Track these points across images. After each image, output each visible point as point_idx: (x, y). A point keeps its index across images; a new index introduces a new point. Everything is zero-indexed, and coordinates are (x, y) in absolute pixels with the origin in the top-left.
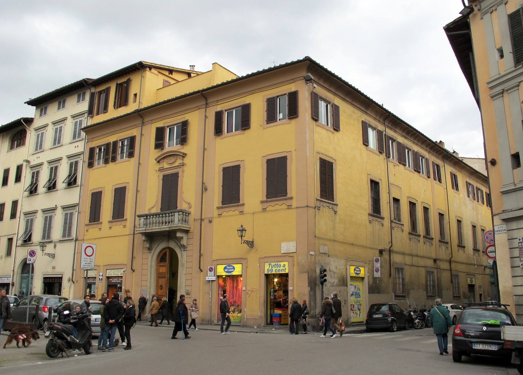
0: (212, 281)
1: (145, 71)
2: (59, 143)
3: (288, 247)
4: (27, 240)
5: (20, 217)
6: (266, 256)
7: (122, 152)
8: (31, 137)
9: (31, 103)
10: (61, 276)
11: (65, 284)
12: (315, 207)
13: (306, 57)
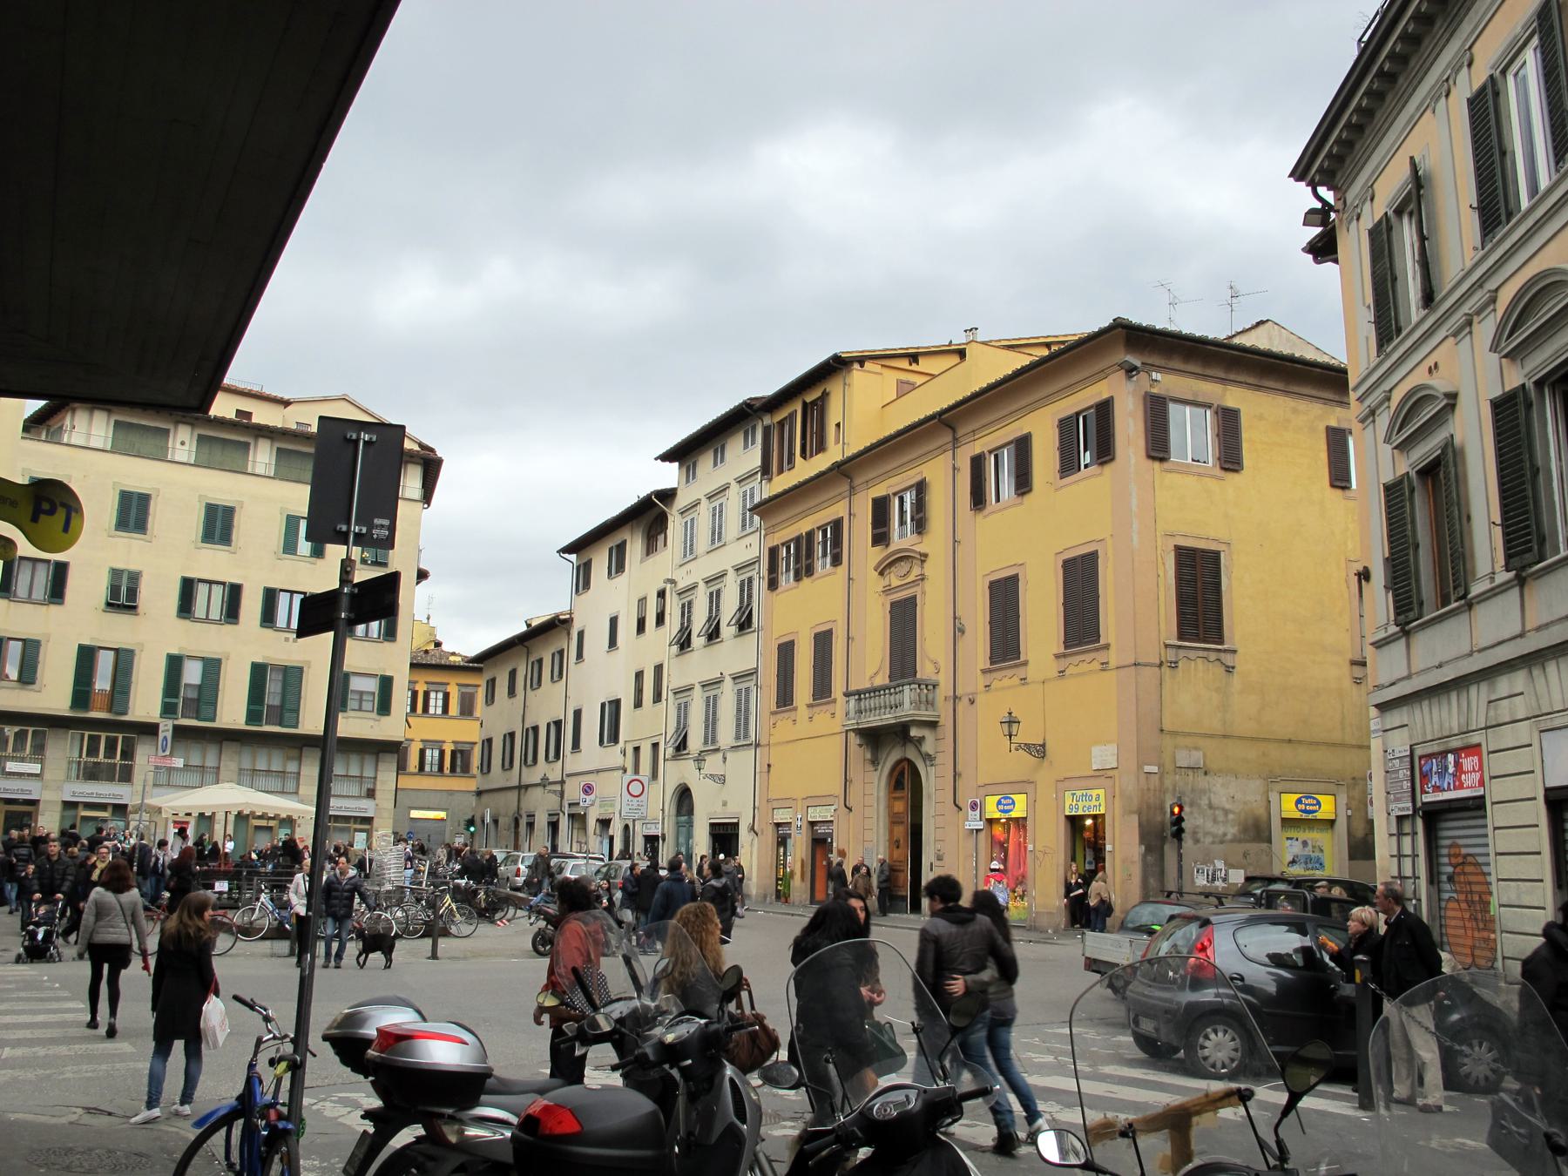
0: (977, 830)
1: (850, 371)
2: (720, 539)
3: (1103, 756)
4: (681, 746)
5: (667, 700)
6: (1069, 775)
7: (902, 522)
8: (675, 526)
9: (668, 457)
10: (735, 821)
11: (744, 836)
12: (1161, 664)
13: (1114, 320)
